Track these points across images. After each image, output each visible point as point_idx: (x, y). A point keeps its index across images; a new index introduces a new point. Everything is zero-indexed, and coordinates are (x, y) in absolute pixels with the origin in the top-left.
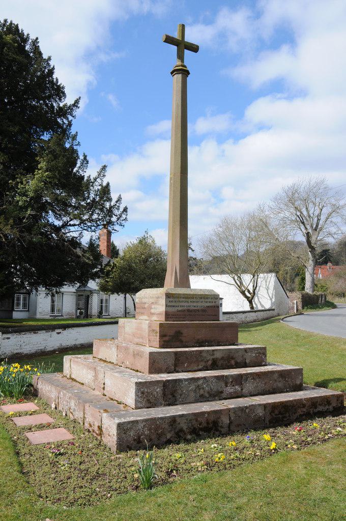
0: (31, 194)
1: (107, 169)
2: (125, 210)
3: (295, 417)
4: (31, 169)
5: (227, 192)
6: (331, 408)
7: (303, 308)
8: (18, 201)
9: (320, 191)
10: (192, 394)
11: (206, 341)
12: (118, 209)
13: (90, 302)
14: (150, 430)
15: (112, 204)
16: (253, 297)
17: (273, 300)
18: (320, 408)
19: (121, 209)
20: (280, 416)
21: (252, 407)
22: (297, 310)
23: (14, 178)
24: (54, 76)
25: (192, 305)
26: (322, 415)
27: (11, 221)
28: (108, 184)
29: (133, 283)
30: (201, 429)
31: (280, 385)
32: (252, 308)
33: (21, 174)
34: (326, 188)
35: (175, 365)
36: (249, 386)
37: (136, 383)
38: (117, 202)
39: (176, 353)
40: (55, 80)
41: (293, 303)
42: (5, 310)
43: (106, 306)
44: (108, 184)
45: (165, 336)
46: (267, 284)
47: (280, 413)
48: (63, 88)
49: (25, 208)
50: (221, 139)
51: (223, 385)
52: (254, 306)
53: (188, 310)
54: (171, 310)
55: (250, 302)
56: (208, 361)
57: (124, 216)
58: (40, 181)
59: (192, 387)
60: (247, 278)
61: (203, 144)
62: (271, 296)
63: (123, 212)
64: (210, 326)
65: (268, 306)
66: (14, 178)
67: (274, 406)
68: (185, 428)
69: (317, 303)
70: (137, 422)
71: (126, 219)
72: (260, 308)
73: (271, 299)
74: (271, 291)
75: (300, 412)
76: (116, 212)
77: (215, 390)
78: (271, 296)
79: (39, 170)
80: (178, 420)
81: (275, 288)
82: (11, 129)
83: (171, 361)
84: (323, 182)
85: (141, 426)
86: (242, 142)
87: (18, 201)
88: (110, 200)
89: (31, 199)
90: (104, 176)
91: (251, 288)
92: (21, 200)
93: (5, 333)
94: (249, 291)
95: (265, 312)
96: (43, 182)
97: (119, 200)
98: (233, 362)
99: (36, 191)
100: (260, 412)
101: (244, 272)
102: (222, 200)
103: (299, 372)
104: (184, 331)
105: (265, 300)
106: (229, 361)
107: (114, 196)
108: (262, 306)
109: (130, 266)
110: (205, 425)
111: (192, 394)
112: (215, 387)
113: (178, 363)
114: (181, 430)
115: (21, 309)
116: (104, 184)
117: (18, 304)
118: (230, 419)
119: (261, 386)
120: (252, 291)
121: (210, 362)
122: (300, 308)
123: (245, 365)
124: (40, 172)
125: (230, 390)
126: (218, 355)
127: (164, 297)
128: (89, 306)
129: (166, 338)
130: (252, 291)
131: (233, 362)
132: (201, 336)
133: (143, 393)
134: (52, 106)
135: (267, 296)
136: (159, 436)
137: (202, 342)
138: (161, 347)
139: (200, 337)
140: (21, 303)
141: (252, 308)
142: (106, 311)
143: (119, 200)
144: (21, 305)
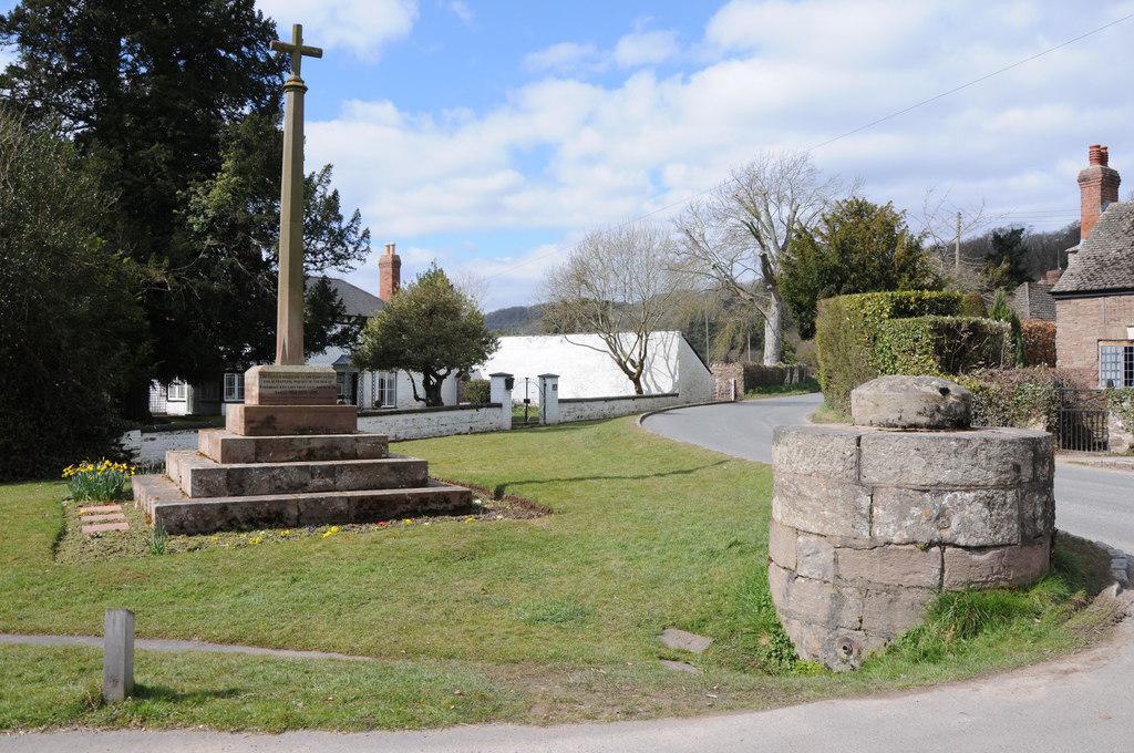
0: (211, 213)
1: (333, 170)
2: (366, 234)
3: (394, 513)
4: (212, 170)
5: (674, 173)
6: (450, 506)
7: (746, 392)
8: (192, 225)
9: (801, 176)
10: (266, 486)
11: (310, 428)
12: (356, 233)
13: (359, 385)
14: (195, 515)
15: (344, 225)
16: (640, 373)
17: (677, 378)
18: (434, 506)
19: (360, 234)
20: (372, 512)
21: (331, 500)
22: (736, 396)
23: (185, 187)
24: (256, 8)
25: (296, 386)
26: (434, 513)
27: (166, 262)
28: (336, 193)
29: (402, 352)
30: (261, 520)
31: (392, 480)
32: (640, 391)
33: (198, 179)
34: (811, 170)
35: (257, 454)
36: (344, 479)
37: (192, 470)
38: (353, 221)
39: (257, 441)
40: (257, 15)
41: (729, 383)
42: (211, 402)
43: (390, 393)
44: (336, 193)
45: (253, 422)
46: (667, 348)
47: (370, 508)
48: (274, 25)
49: (200, 236)
50: (663, 72)
51: (309, 476)
52: (644, 387)
53: (291, 392)
54: (267, 392)
55: (637, 382)
56: (301, 451)
57: (364, 245)
58: (226, 189)
59: (266, 477)
60: (629, 340)
61: (628, 84)
62: (672, 370)
63: (362, 238)
64: (326, 410)
65: (667, 389)
66: (185, 187)
67: (362, 500)
68: (239, 516)
69: (782, 384)
70: (179, 507)
71: (368, 249)
72: (654, 392)
73: (673, 377)
74: (673, 362)
75: (401, 508)
76: (353, 237)
77: (297, 481)
78: (672, 370)
79: (223, 172)
80: (230, 508)
81: (680, 357)
82: (181, 105)
83: (251, 450)
84: (804, 159)
85: (184, 511)
86: (695, 78)
87: (192, 225)
88: (339, 218)
89: (214, 219)
90: (328, 181)
91: (636, 359)
92: (197, 223)
93: (147, 432)
94: (633, 362)
95: (657, 399)
96: (230, 192)
97: (356, 218)
98: (337, 453)
99: (218, 208)
100: (342, 506)
101: (627, 328)
102: (666, 190)
103: (423, 465)
104: (279, 417)
105: (661, 379)
106: (330, 451)
107: (346, 211)
108: (659, 388)
109: (399, 322)
110: (264, 514)
111: (266, 486)
112: (296, 478)
113: (260, 452)
114: (235, 519)
115: (236, 400)
116: (329, 193)
117: (231, 392)
118: (299, 510)
119: (363, 479)
120: (637, 364)
121: (304, 453)
122: (741, 391)
123: (356, 457)
124: (225, 175)
125: (318, 482)
126: (316, 444)
127: (258, 376)
128: (359, 392)
129: (253, 425)
130: (637, 364)
131: (337, 453)
132: (303, 422)
133: (201, 481)
134: (255, 58)
135: (665, 371)
136: (207, 523)
137: (304, 429)
138: (246, 435)
139: (301, 423)
140: (236, 389)
141: (640, 391)
142: (390, 401)
143: (356, 218)
144: (236, 392)
